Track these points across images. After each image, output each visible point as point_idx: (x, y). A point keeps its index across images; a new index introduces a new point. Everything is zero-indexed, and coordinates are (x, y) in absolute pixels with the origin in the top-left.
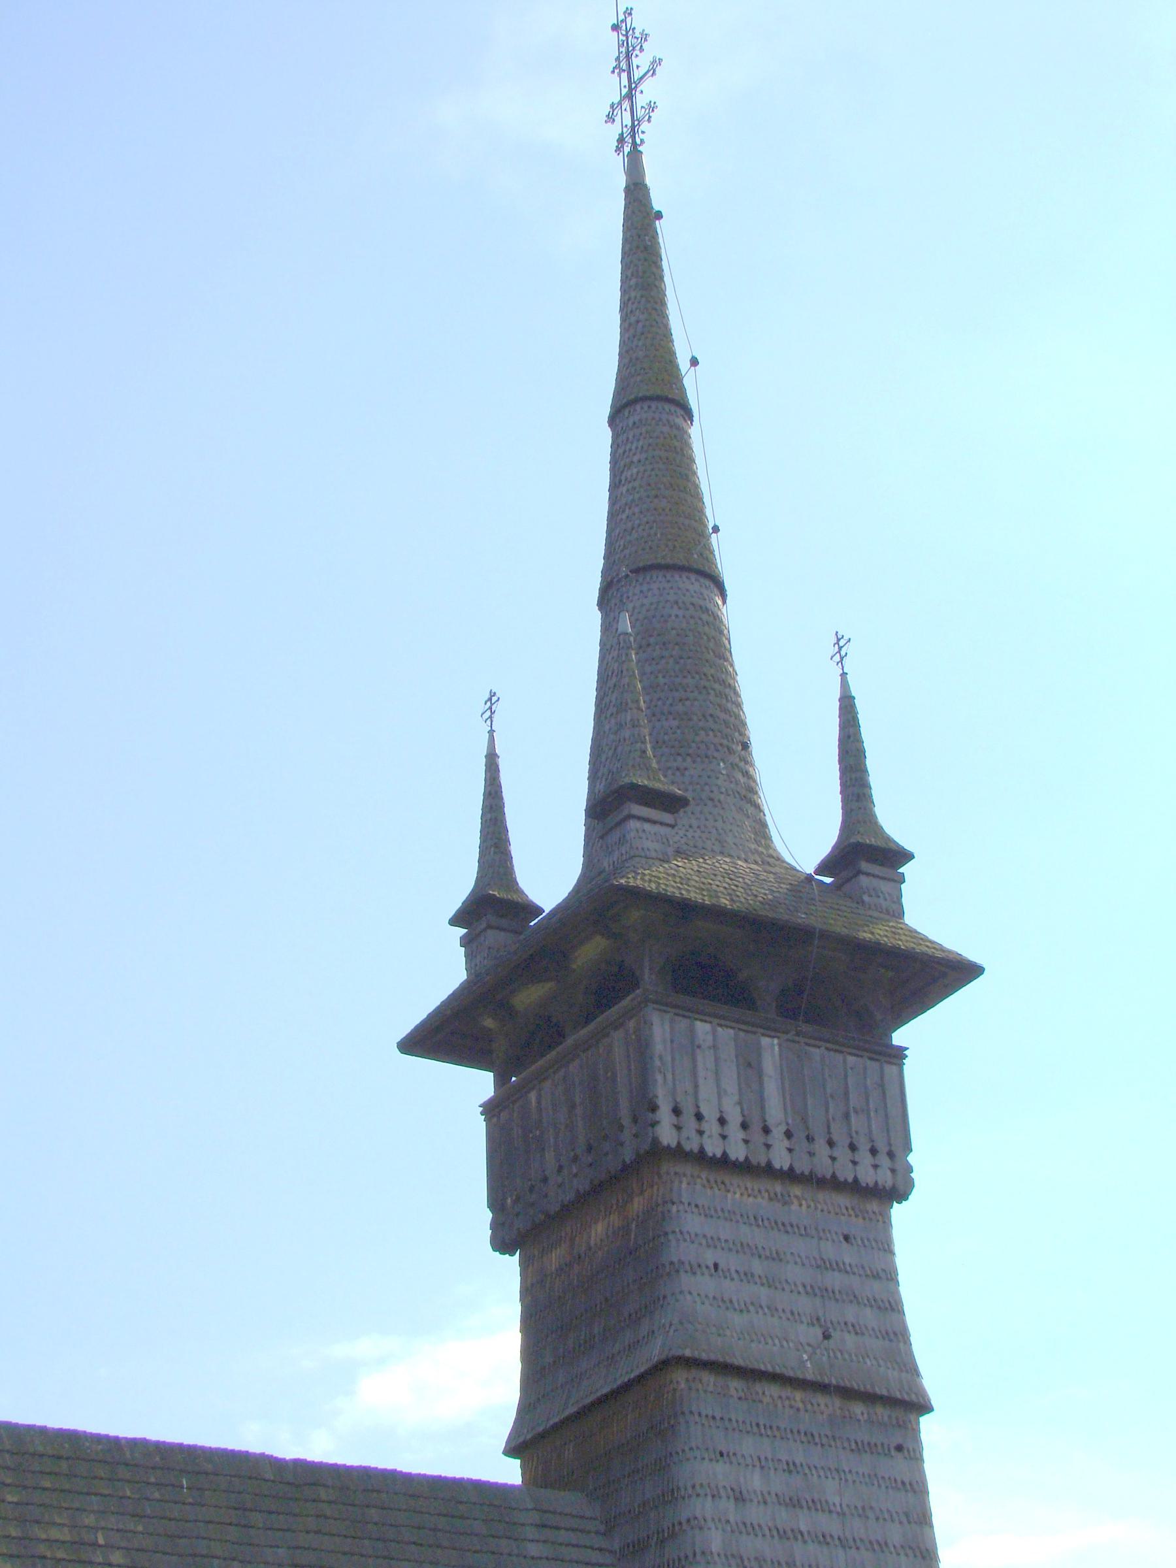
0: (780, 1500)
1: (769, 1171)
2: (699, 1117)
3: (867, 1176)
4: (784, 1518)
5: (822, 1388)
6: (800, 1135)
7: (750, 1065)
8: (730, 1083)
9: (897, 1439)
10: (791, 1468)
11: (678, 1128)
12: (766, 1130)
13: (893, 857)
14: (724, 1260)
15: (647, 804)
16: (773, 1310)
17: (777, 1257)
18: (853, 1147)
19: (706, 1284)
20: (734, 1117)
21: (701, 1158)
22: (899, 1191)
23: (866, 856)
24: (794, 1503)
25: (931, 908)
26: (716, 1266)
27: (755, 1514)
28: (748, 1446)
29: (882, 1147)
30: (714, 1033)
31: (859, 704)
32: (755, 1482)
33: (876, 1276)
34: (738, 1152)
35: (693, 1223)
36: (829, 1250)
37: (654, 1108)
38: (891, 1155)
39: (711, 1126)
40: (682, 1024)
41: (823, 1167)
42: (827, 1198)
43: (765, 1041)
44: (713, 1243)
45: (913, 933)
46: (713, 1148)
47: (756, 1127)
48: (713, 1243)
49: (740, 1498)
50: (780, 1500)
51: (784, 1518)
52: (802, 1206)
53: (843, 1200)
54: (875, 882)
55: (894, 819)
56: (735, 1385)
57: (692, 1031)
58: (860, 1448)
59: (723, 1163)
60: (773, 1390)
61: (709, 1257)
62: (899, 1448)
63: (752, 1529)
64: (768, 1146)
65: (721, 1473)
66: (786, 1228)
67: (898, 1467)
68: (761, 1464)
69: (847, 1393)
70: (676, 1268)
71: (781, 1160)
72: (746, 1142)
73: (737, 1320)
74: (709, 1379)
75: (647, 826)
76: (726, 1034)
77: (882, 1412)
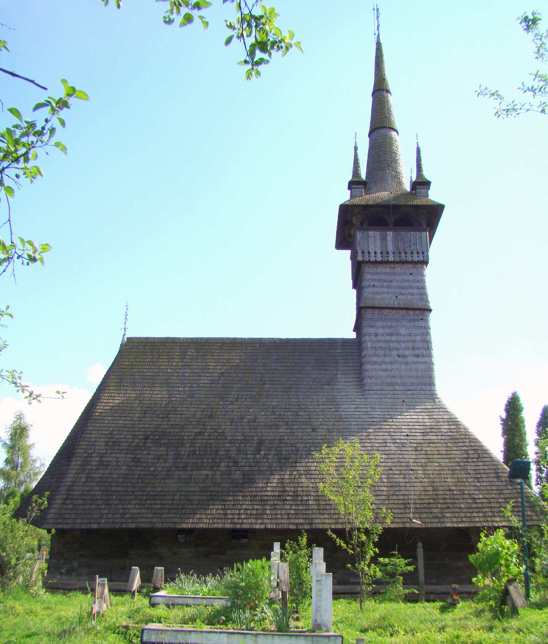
0: (388, 334)
1: (388, 262)
2: (369, 253)
3: (416, 259)
4: (388, 338)
5: (408, 309)
6: (397, 253)
7: (384, 239)
8: (378, 243)
9: (421, 317)
10: (391, 327)
11: (363, 256)
12: (388, 253)
13: (427, 184)
14: (375, 283)
15: (356, 185)
16: (388, 293)
17: (391, 281)
18: (412, 253)
19: (371, 290)
20: (378, 251)
21: (369, 262)
22: (425, 262)
23: (421, 184)
24: (391, 335)
25: (434, 195)
26: (374, 286)
27: (380, 338)
28: (379, 324)
29: (420, 251)
30: (374, 233)
31: (421, 149)
32: (381, 331)
33: (418, 282)
34: (379, 259)
35: (368, 277)
36: (405, 277)
37: (357, 253)
38: (423, 253)
39: (372, 254)
40: (366, 232)
41: (403, 258)
42: (405, 266)
43: (388, 233)
44: (374, 280)
45: (431, 201)
46: (372, 259)
47: (385, 253)
48: (374, 280)
49: (376, 335)
50: (388, 334)
51: (388, 338)
52: (399, 269)
53: (410, 266)
54: (420, 190)
55: (427, 175)
56: (377, 311)
57: (368, 234)
58: (410, 321)
59: (376, 262)
60: (386, 311)
61: (372, 284)
62: (422, 319)
63: (379, 341)
64: (388, 257)
65: (372, 330)
66: (393, 274)
67: (422, 324)
68: (383, 327)
69: (408, 309)
70: (364, 287)
71: (391, 259)
72: (382, 256)
73: (379, 297)
74: (370, 311)
75: (357, 190)
76: (377, 233)
77: (418, 312)
